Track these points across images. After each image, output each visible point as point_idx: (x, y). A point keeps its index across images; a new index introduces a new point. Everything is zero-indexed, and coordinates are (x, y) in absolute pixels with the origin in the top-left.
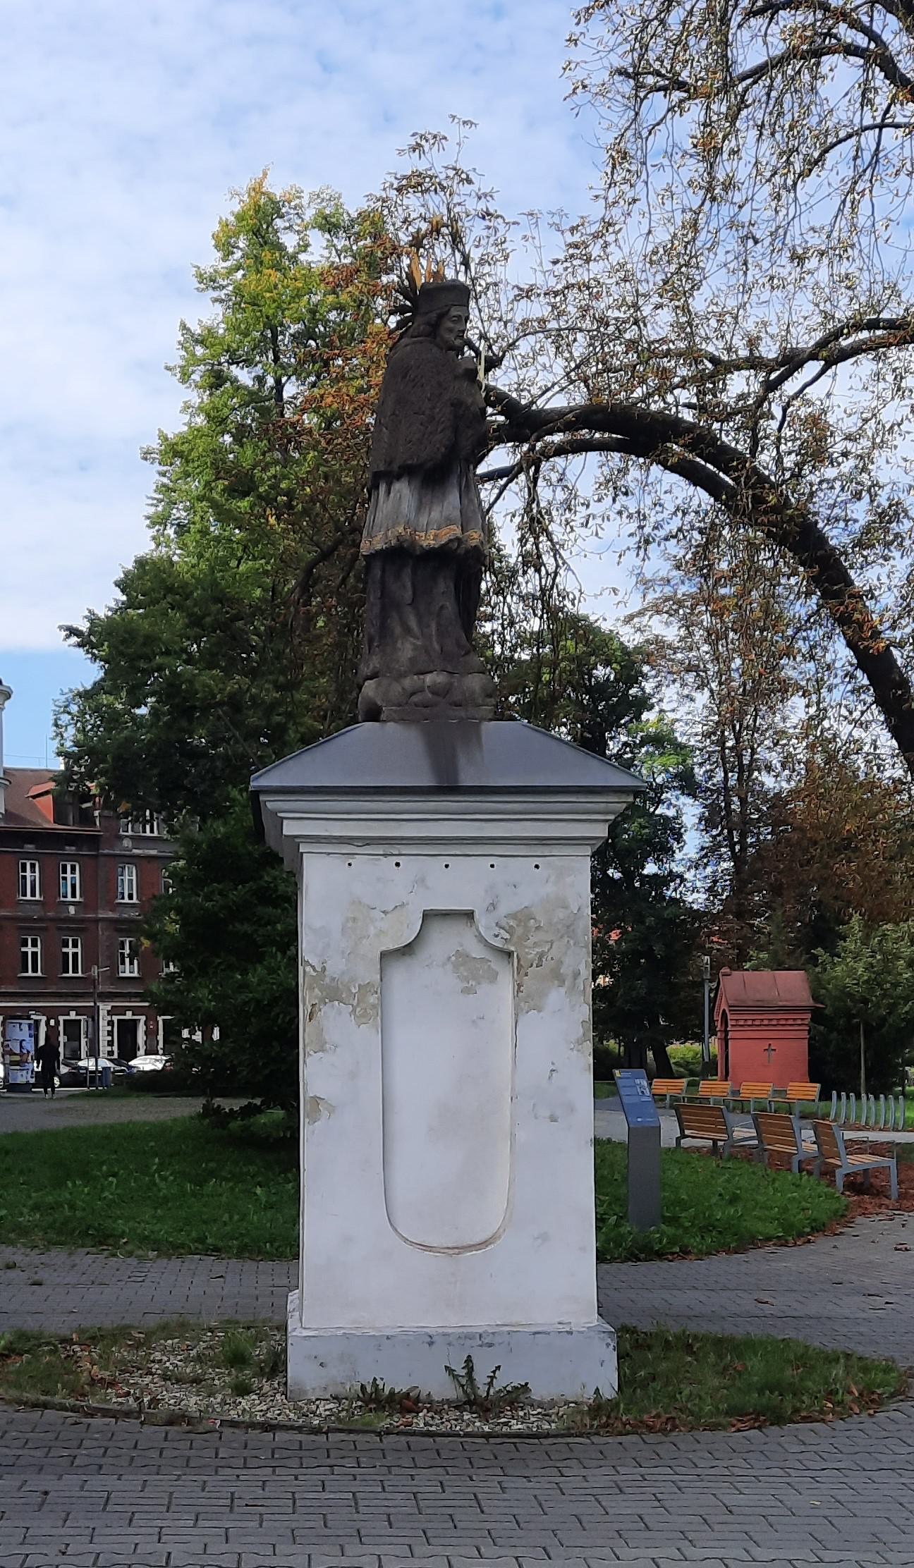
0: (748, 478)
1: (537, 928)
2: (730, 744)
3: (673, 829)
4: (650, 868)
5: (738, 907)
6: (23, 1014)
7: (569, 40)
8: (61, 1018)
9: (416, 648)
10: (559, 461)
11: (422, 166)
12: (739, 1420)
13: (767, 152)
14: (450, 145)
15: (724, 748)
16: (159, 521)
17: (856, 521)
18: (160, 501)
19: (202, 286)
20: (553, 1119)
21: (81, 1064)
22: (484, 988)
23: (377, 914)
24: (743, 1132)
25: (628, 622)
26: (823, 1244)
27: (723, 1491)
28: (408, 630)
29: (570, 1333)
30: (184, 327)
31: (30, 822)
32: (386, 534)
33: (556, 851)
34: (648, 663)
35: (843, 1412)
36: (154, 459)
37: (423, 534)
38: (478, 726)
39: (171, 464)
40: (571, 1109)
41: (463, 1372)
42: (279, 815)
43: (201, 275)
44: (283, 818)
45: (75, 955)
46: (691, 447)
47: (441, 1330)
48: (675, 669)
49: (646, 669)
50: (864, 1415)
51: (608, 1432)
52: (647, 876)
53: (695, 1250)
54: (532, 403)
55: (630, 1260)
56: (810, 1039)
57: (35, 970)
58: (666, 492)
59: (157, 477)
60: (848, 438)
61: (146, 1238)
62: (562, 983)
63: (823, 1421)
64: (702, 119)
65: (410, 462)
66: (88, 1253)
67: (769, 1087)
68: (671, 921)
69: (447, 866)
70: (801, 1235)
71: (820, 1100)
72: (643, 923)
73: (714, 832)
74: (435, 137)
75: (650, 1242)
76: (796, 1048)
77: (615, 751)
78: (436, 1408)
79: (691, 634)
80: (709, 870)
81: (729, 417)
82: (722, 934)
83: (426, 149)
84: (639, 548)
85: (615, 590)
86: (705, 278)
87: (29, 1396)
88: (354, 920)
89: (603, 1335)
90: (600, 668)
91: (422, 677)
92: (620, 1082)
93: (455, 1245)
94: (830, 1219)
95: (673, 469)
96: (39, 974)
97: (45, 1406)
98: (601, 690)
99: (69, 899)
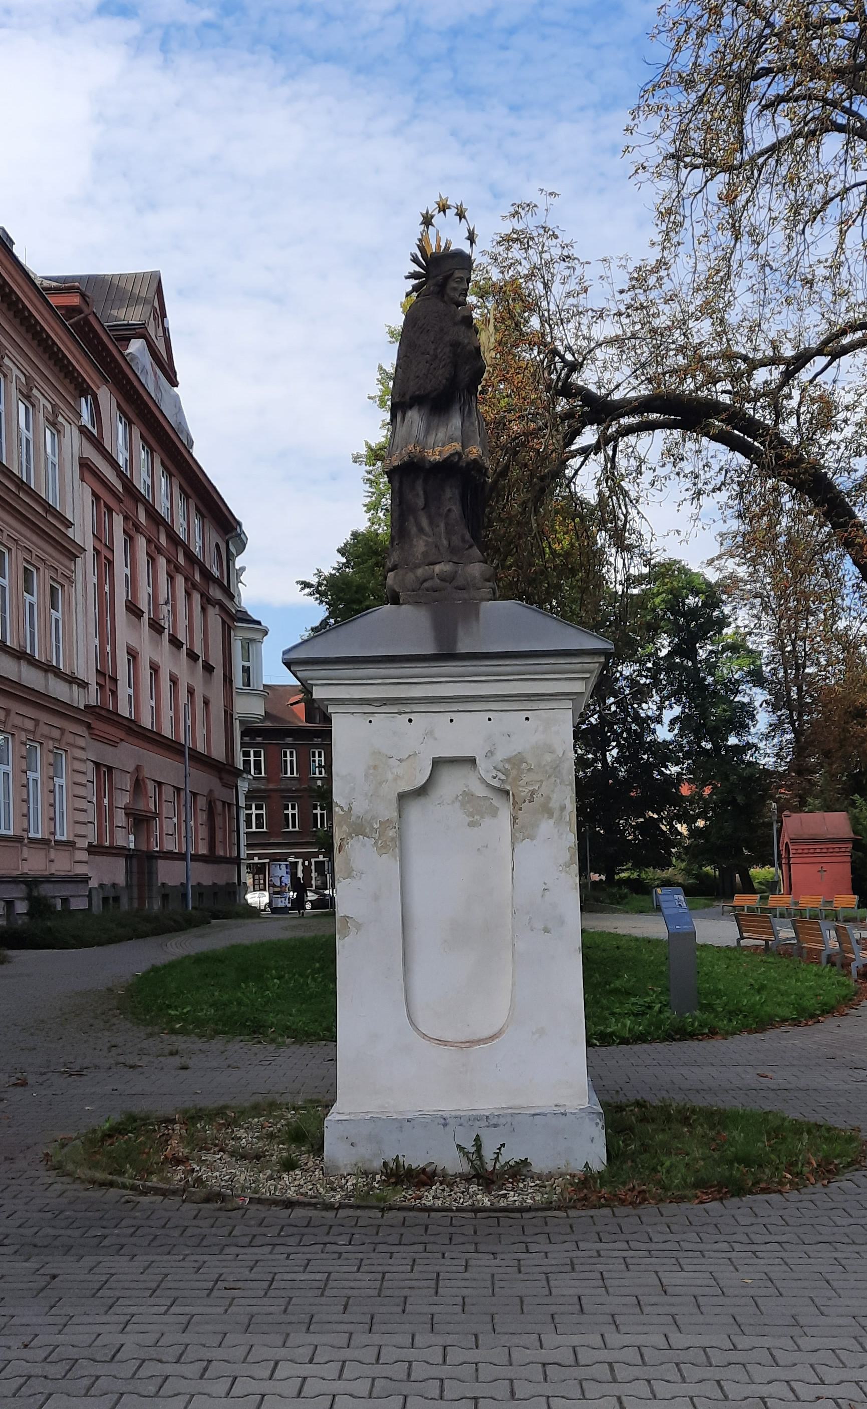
0: (771, 442)
1: (530, 770)
2: (788, 649)
3: (747, 712)
4: (733, 740)
5: (799, 768)
6: (283, 858)
7: (627, 130)
8: (313, 860)
9: (427, 544)
10: (631, 439)
11: (519, 227)
12: (703, 1193)
13: (781, 208)
14: (541, 211)
15: (783, 652)
16: (372, 507)
17: (856, 471)
18: (373, 493)
19: (394, 339)
20: (546, 930)
21: (327, 892)
22: (487, 821)
23: (395, 763)
24: (786, 933)
25: (710, 564)
26: (830, 1023)
27: (665, 1268)
28: (421, 530)
29: (564, 1114)
30: (381, 368)
31: (289, 722)
32: (401, 453)
33: (541, 705)
34: (725, 593)
35: (799, 1182)
36: (362, 461)
37: (430, 451)
38: (477, 604)
39: (374, 465)
40: (562, 922)
41: (473, 1150)
42: (309, 682)
43: (392, 332)
44: (313, 685)
45: (294, 815)
46: (727, 421)
47: (453, 1113)
48: (745, 597)
49: (724, 597)
50: (819, 1185)
51: (584, 1205)
52: (730, 746)
53: (722, 1031)
54: (608, 395)
55: (667, 1040)
56: (852, 863)
57: (294, 826)
58: (712, 457)
59: (366, 474)
60: (847, 408)
61: (288, 1028)
62: (551, 815)
63: (780, 1192)
64: (727, 181)
65: (417, 393)
66: (242, 1041)
67: (821, 898)
68: (750, 778)
69: (451, 721)
70: (812, 1016)
71: (859, 907)
72: (728, 780)
73: (779, 713)
74: (529, 205)
75: (684, 1025)
76: (842, 870)
77: (704, 657)
78: (448, 1181)
79: (756, 571)
80: (776, 740)
81: (755, 400)
82: (789, 787)
83: (523, 215)
84: (693, 499)
85: (678, 532)
86: (735, 299)
87: (100, 1175)
88: (375, 767)
89: (592, 1116)
90: (690, 597)
91: (432, 567)
92: (661, 898)
93: (467, 1039)
94: (839, 1002)
95: (715, 438)
96: (297, 829)
97: (111, 1184)
98: (693, 613)
99: (317, 775)
